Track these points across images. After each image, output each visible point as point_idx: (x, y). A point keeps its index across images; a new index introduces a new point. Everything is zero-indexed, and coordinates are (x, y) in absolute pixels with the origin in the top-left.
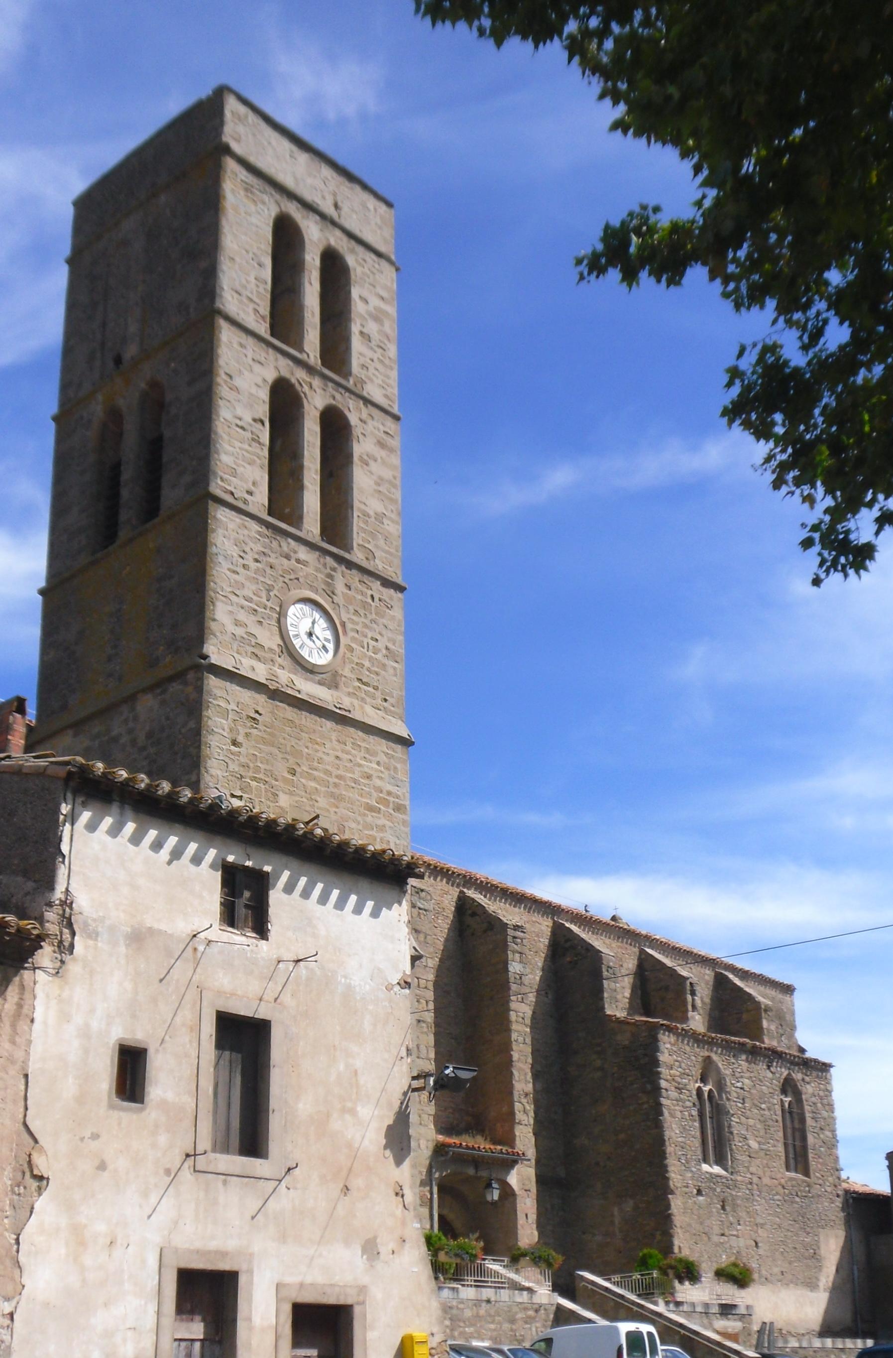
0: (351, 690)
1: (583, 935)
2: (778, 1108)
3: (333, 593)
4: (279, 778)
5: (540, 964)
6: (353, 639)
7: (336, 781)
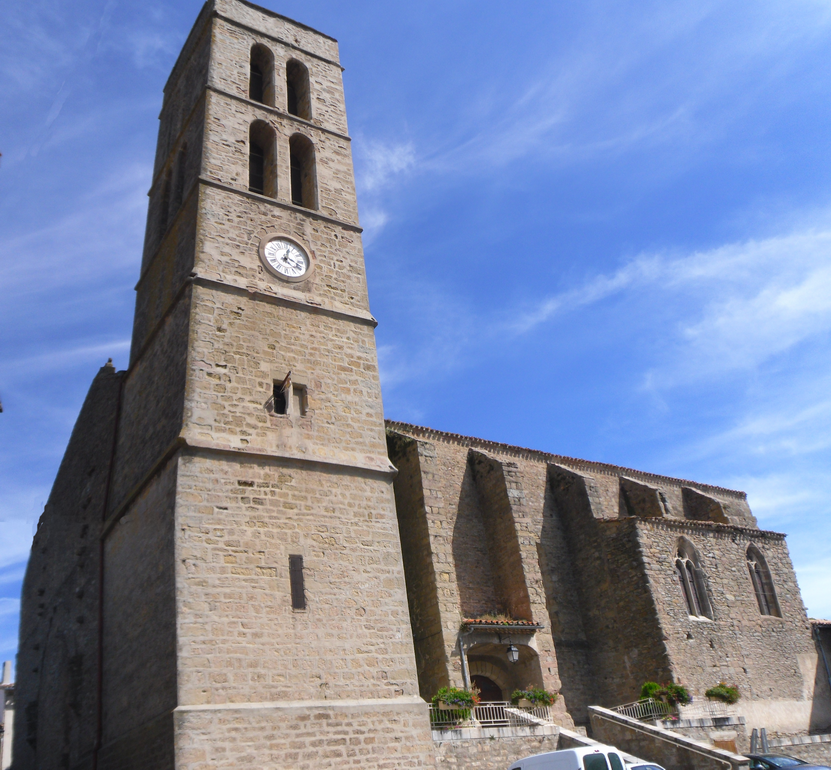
1: (570, 469)
2: (746, 569)
4: (261, 351)
5: (542, 495)
6: (321, 261)
7: (313, 351)
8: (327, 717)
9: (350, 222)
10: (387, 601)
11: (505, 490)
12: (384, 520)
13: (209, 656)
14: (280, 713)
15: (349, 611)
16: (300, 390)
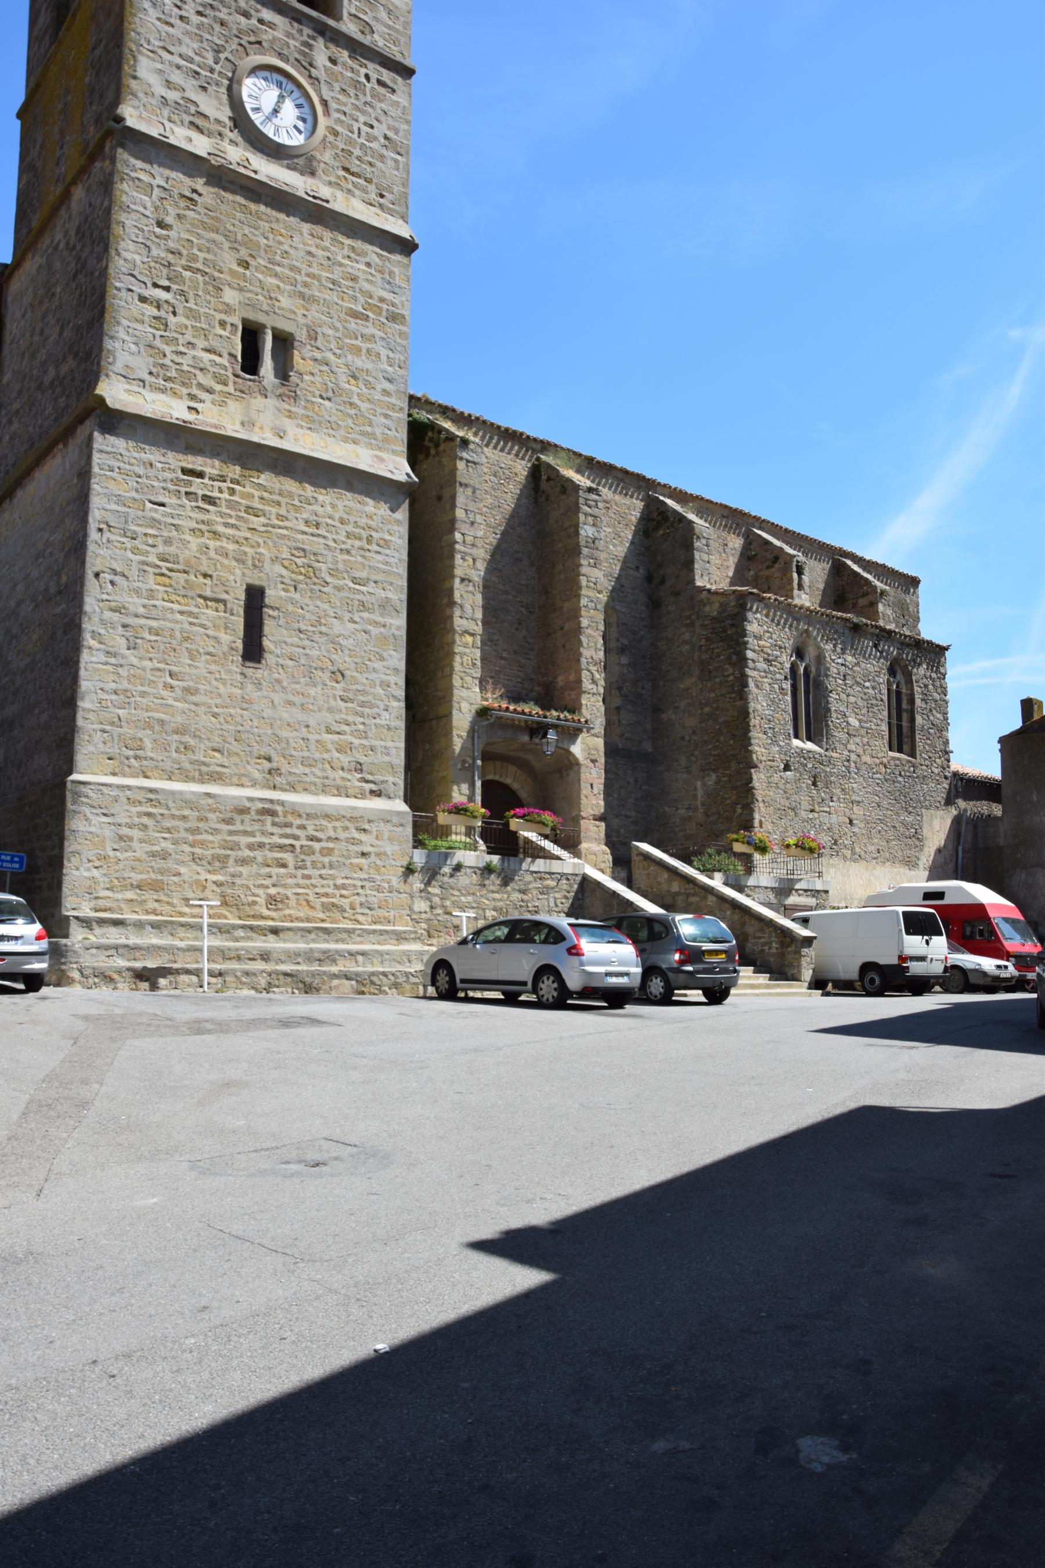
0: (333, 179)
3: (311, 65)
4: (225, 270)
6: (338, 121)
7: (308, 280)
8: (273, 813)
9: (394, 52)
10: (376, 665)
11: (576, 527)
12: (388, 552)
13: (120, 712)
14: (210, 801)
15: (321, 674)
16: (284, 342)
